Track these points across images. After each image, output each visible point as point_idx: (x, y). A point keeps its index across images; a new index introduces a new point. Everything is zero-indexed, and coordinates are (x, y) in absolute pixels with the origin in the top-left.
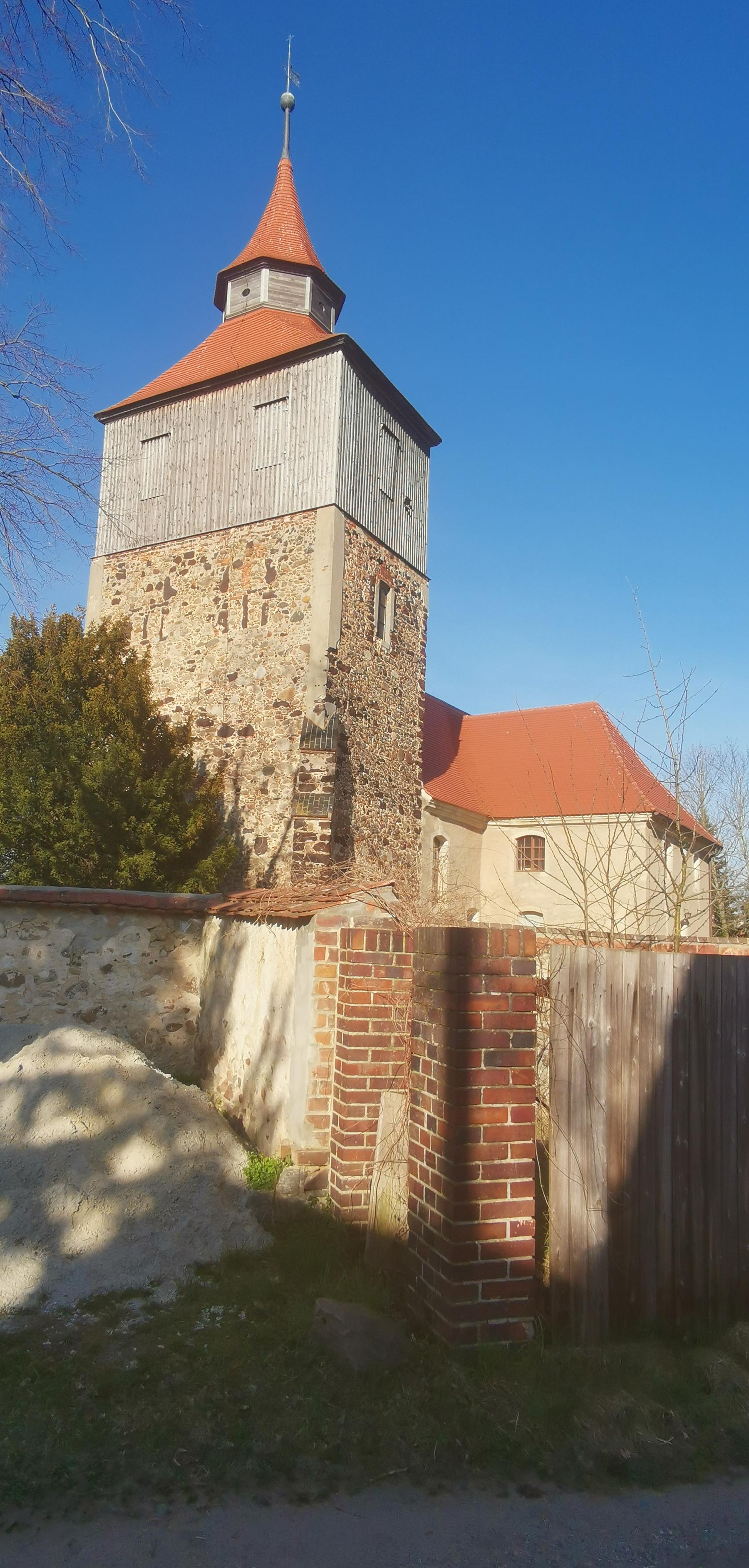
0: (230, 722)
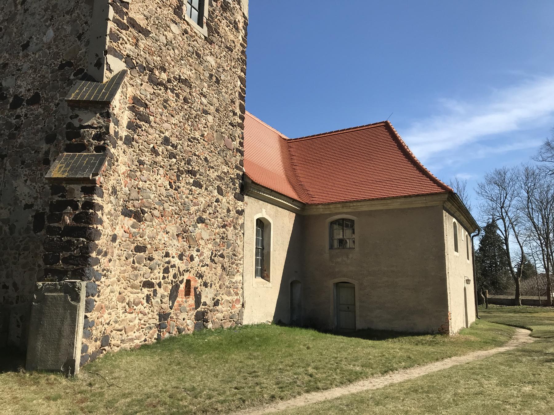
0: (21, 92)
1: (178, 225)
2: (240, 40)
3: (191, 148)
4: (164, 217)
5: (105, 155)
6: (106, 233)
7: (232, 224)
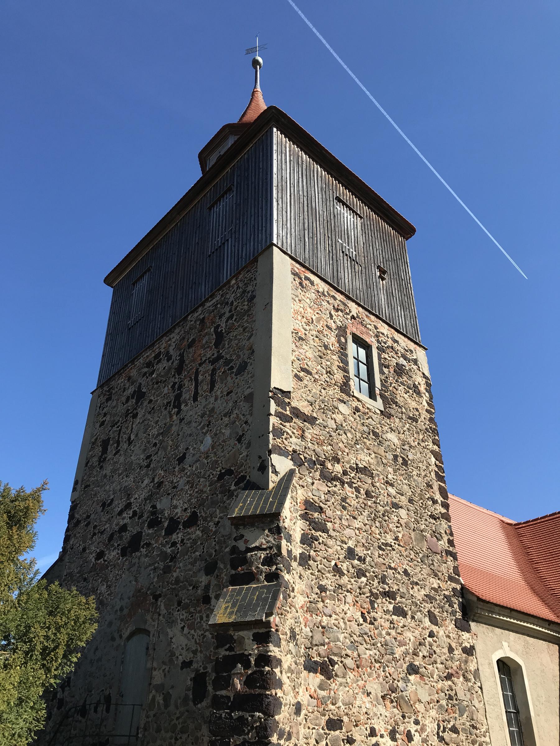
0: (177, 513)
1: (381, 679)
2: (424, 406)
3: (384, 559)
4: (360, 669)
5: (279, 585)
6: (288, 702)
7: (461, 673)
